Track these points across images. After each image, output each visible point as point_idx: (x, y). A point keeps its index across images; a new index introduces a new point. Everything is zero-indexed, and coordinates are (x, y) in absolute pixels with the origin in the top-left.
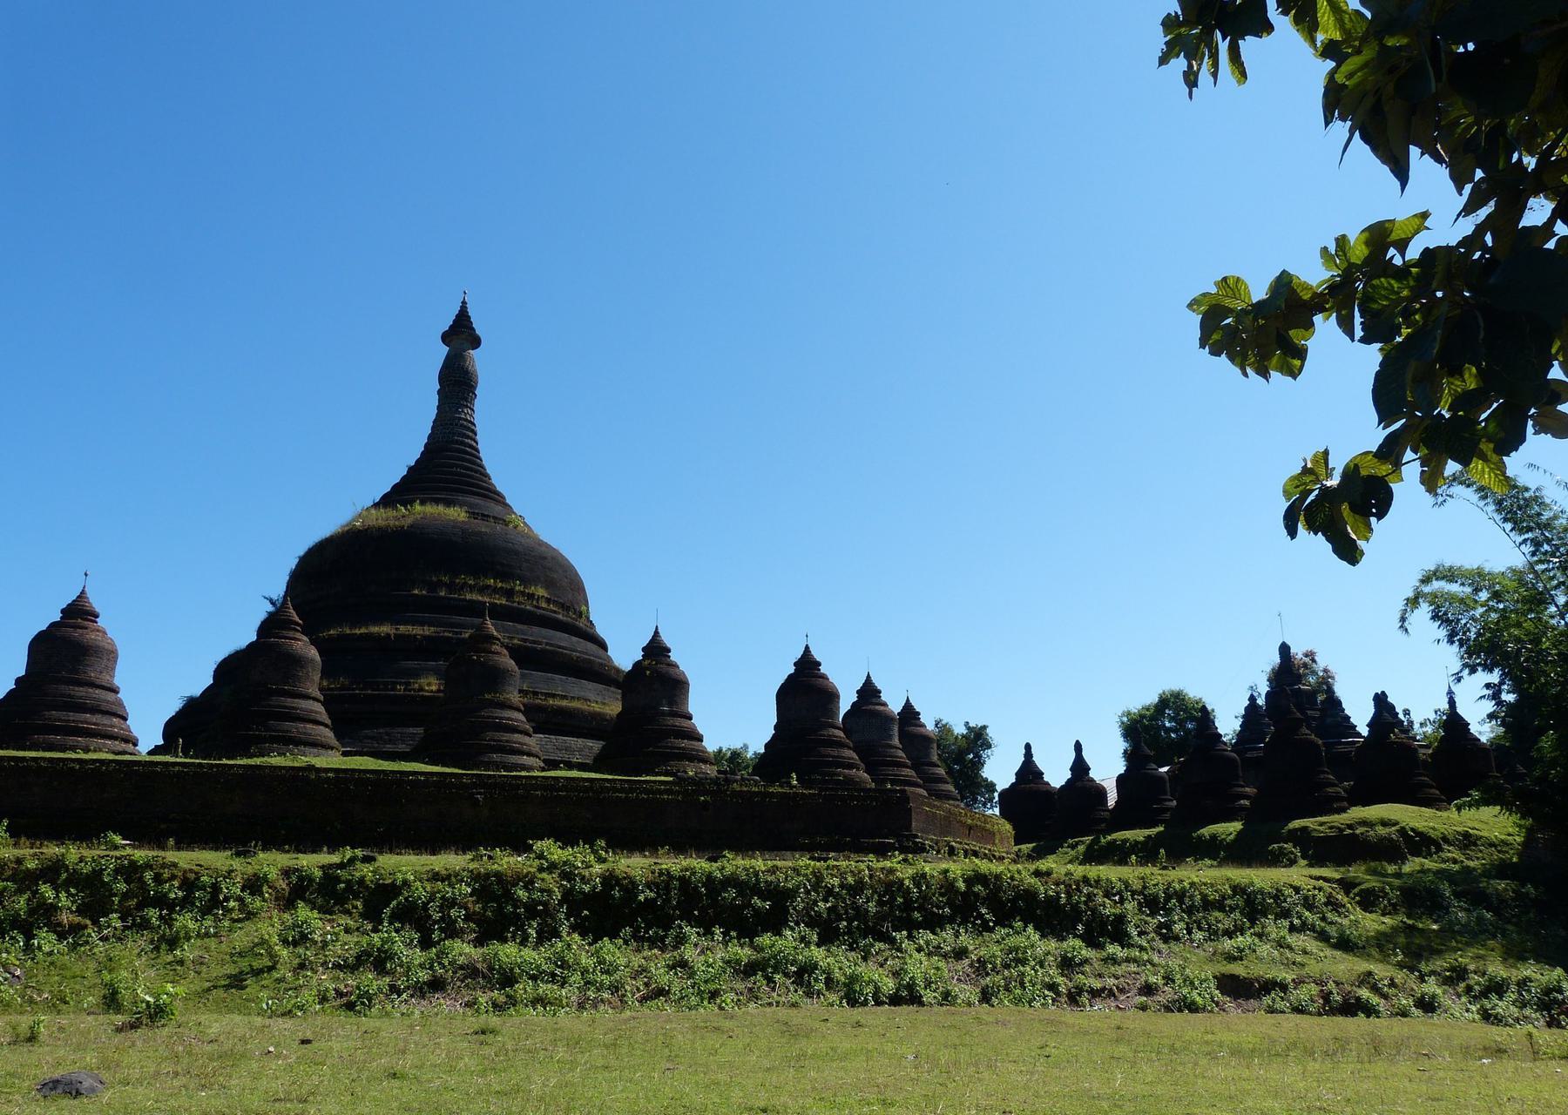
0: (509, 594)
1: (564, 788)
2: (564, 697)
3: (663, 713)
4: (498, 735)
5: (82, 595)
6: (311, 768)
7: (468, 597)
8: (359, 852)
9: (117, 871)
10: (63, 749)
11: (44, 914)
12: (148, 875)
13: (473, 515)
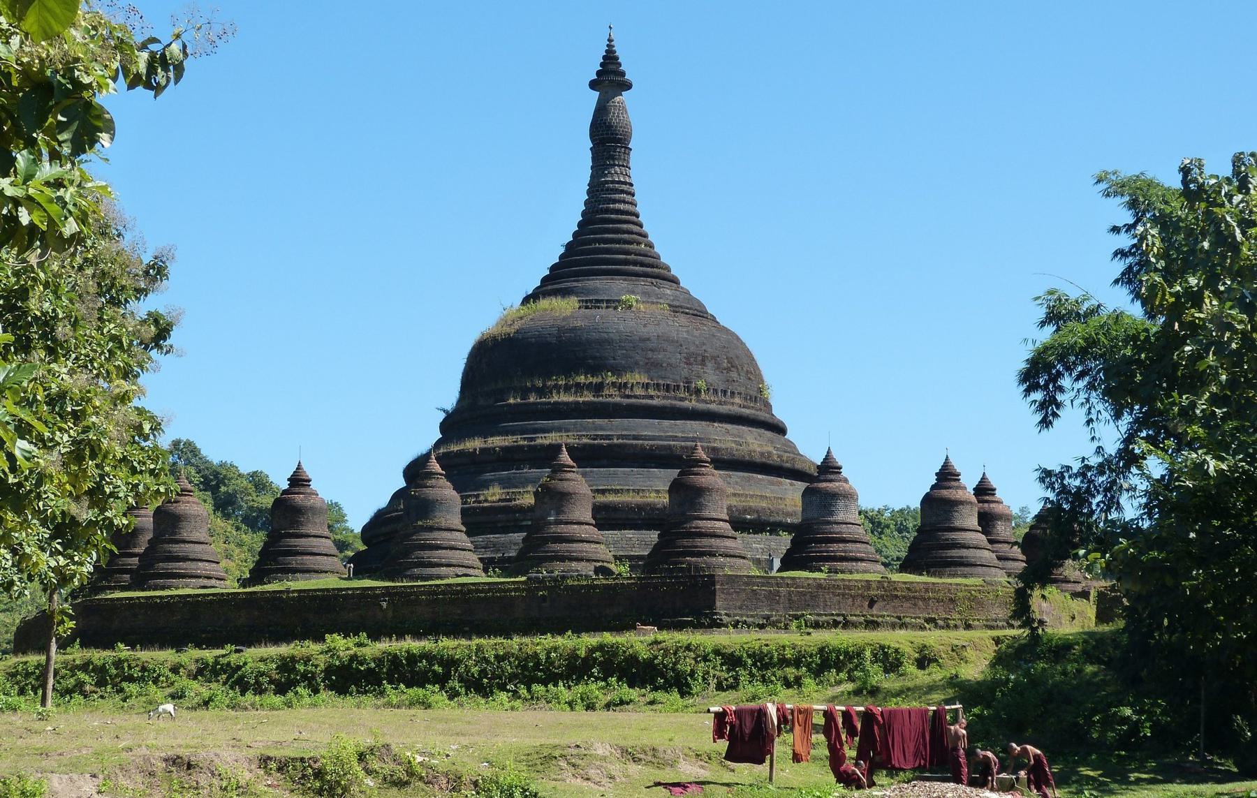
0: (598, 388)
2: (617, 492)
4: (557, 547)
5: (984, 478)
6: (288, 591)
7: (555, 398)
8: (233, 647)
9: (113, 664)
10: (163, 588)
11: (80, 686)
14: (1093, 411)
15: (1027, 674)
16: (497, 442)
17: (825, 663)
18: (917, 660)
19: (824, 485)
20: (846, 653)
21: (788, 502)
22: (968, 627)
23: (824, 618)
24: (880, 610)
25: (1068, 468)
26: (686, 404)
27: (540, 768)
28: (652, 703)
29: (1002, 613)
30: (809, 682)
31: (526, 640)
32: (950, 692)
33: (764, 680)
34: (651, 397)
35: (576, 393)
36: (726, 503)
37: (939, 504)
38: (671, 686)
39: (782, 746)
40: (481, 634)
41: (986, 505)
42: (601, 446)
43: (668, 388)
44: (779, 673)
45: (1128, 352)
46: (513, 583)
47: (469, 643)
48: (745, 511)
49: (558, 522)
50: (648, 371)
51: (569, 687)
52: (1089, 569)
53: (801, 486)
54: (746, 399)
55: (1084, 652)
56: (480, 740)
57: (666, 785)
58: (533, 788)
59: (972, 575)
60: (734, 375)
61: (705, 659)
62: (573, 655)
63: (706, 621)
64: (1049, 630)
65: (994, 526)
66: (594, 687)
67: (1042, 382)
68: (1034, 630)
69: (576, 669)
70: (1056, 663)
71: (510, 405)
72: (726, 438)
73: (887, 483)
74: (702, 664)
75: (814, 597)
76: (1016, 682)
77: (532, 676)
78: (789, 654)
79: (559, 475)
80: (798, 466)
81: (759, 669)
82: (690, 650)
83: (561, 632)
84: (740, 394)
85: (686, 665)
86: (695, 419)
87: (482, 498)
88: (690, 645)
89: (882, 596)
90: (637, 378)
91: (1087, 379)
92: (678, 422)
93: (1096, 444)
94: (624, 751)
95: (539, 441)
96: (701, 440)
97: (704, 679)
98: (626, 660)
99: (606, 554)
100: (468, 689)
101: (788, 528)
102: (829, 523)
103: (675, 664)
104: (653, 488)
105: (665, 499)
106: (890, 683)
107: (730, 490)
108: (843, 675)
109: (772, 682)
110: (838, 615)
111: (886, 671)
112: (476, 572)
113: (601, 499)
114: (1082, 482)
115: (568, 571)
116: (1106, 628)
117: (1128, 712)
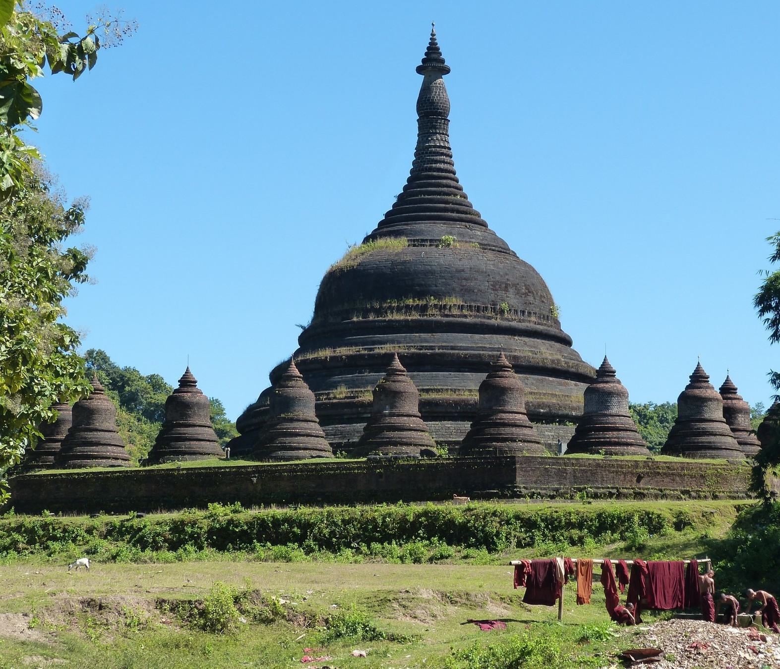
0: (423, 309)
1: (301, 471)
2: (438, 391)
3: (385, 416)
4: (391, 434)
5: (728, 380)
7: (390, 317)
8: (136, 514)
10: (80, 467)
12: (51, 527)
13: (415, 243)
15: (762, 534)
16: (344, 351)
17: (603, 526)
18: (675, 523)
19: (601, 385)
20: (619, 518)
21: (573, 399)
22: (715, 497)
23: (602, 490)
26: (493, 321)
27: (377, 608)
28: (466, 557)
29: (742, 486)
30: (589, 541)
31: (367, 508)
32: (701, 549)
34: (465, 316)
35: (406, 313)
36: (524, 399)
37: (692, 401)
39: (568, 592)
40: (330, 503)
41: (729, 401)
42: (425, 355)
43: (478, 309)
44: (566, 534)
46: (356, 462)
47: (321, 510)
48: (540, 406)
49: (392, 415)
50: (462, 296)
51: (401, 545)
53: (584, 386)
54: (540, 317)
56: (330, 586)
58: (372, 624)
60: (531, 299)
61: (508, 522)
62: (404, 520)
63: (509, 493)
65: (736, 418)
66: (420, 544)
69: (406, 531)
71: (354, 321)
72: (524, 348)
73: (650, 385)
74: (506, 527)
75: (594, 474)
77: (372, 535)
78: (574, 518)
80: (581, 370)
81: (551, 531)
82: (496, 516)
83: (394, 501)
84: (535, 313)
85: (493, 527)
87: (332, 396)
88: (495, 511)
89: (647, 473)
90: (453, 301)
92: (486, 336)
94: (444, 595)
95: (377, 351)
96: (504, 350)
97: (507, 538)
98: (445, 523)
100: (320, 546)
101: (573, 419)
103: (484, 527)
104: (467, 388)
105: (476, 397)
106: (654, 541)
107: (528, 390)
109: (560, 541)
110: (612, 488)
115: (400, 453)
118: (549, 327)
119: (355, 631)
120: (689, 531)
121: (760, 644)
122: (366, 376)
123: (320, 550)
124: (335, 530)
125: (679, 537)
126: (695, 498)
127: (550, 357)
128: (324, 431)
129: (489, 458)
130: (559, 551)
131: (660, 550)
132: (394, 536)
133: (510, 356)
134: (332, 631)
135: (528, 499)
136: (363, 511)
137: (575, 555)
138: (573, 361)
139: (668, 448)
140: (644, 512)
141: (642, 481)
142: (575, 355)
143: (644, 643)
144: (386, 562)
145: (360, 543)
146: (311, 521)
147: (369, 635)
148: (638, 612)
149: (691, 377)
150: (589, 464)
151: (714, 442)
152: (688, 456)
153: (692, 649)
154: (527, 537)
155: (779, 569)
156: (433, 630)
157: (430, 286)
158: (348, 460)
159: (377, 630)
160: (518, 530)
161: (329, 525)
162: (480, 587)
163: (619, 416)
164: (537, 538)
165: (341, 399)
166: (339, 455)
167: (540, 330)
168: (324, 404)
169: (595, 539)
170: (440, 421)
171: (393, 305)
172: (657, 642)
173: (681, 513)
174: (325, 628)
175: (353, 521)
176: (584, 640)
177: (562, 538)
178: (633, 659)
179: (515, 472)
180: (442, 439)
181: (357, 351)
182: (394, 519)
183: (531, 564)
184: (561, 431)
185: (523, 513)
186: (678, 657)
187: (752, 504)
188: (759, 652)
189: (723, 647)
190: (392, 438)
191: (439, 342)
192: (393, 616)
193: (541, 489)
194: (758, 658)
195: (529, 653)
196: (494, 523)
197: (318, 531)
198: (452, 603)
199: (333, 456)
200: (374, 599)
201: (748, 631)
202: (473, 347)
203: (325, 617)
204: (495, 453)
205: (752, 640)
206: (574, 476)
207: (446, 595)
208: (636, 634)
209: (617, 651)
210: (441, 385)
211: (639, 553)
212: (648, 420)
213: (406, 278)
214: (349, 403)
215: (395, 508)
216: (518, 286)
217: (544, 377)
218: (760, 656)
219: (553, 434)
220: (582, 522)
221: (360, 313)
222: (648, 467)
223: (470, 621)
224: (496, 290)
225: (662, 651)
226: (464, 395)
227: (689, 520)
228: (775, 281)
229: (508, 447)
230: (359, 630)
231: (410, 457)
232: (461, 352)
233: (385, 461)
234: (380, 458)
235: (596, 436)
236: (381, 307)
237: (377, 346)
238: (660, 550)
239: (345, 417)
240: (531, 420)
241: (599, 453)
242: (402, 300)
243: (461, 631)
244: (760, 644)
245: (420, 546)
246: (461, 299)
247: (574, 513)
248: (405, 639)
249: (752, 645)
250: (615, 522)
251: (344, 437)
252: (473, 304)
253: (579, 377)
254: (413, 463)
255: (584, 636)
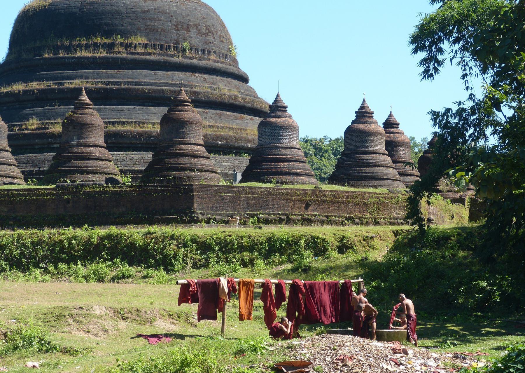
0: (110, 47)
2: (123, 123)
3: (73, 146)
4: (79, 163)
5: (390, 116)
7: (79, 54)
14: (467, 68)
15: (413, 257)
16: (35, 85)
17: (272, 249)
18: (338, 247)
19: (274, 119)
20: (287, 242)
21: (249, 132)
22: (377, 223)
23: (273, 216)
24: (313, 211)
25: (449, 110)
26: (175, 59)
27: (53, 323)
28: (145, 277)
29: (401, 213)
30: (260, 263)
31: (55, 231)
32: (361, 271)
33: (227, 261)
34: (149, 54)
35: (94, 50)
36: (203, 132)
37: (357, 134)
38: (159, 265)
39: (231, 308)
40: (20, 227)
41: (392, 135)
42: (112, 90)
43: (161, 47)
44: (238, 256)
45: (491, 23)
46: (46, 189)
47: (12, 233)
48: (217, 138)
49: (79, 145)
50: (147, 35)
51: (85, 266)
52: (457, 184)
53: (258, 120)
54: (219, 56)
55: (458, 241)
56: (10, 303)
57: (146, 337)
58: (47, 338)
59: (380, 186)
60: (210, 38)
61: (185, 245)
62: (88, 242)
63: (186, 218)
64: (433, 226)
65: (397, 151)
66: (103, 265)
67: (427, 44)
68: (422, 226)
69: (91, 252)
70: (438, 249)
71: (45, 58)
72: (203, 84)
73: (318, 119)
74: (183, 249)
75: (265, 201)
76: (406, 264)
77: (58, 257)
78: (245, 242)
79: (80, 111)
80: (257, 106)
81: (224, 253)
82: (174, 239)
83: (80, 225)
84: (215, 52)
85: (171, 249)
86: (181, 71)
87: (24, 127)
88: (174, 235)
89: (315, 201)
90: (140, 40)
91: (461, 43)
92: (169, 73)
93: (469, 92)
94: (116, 312)
95: (66, 86)
96: (185, 86)
97: (184, 260)
98: (127, 246)
99: (113, 168)
100: (11, 266)
101: (248, 151)
102: (277, 147)
103: (162, 249)
104: (149, 121)
105: (158, 129)
106: (318, 263)
107: (206, 123)
108: (284, 258)
109: (233, 262)
110: (283, 214)
111: (316, 255)
112: (19, 181)
113: (111, 128)
114: (460, 120)
115: (86, 181)
116: (474, 225)
117: (484, 284)
118: (227, 65)
119: (31, 344)
120: (350, 254)
121: (402, 357)
122: (57, 109)
123: (10, 270)
124: (24, 252)
125: (341, 260)
126: (358, 224)
127: (228, 93)
128: (16, 159)
129: (169, 186)
130: (232, 272)
131: (323, 271)
132: (79, 258)
133: (190, 91)
134: (10, 344)
135: (204, 224)
136: (51, 234)
137: (242, 275)
138: (248, 97)
139: (333, 179)
140: (310, 237)
141: (310, 208)
142: (251, 92)
143: (295, 356)
144: (71, 281)
145: (48, 264)
146: (3, 243)
147: (44, 349)
148: (296, 327)
149: (356, 112)
150: (262, 192)
151: (376, 173)
152: (353, 186)
153: (340, 362)
154: (203, 259)
155: (428, 289)
156: (103, 344)
157: (117, 25)
158: (38, 187)
159: (51, 343)
160: (194, 252)
161: (19, 246)
162: (151, 304)
163: (290, 148)
164: (211, 260)
165: (33, 130)
166: (30, 182)
167: (219, 68)
168: (17, 134)
169: (264, 261)
170: (125, 151)
171: (82, 43)
172: (307, 355)
173: (344, 237)
174: (4, 341)
175: (42, 243)
176: (240, 353)
177: (234, 260)
178: (285, 370)
179: (193, 199)
180: (126, 168)
181: (48, 86)
182: (79, 242)
183: (196, 284)
184: (237, 162)
185: (199, 237)
186: (326, 368)
187: (409, 230)
188: (401, 364)
189: (367, 359)
190: (79, 166)
191: (124, 78)
192: (67, 330)
193: (217, 215)
194: (399, 369)
195: (188, 365)
196: (172, 246)
197: (9, 252)
198: (123, 319)
199: (24, 183)
200: (51, 315)
201: (392, 345)
202: (157, 83)
203: (4, 331)
204: (175, 182)
205: (395, 353)
206: (247, 203)
207: (118, 311)
208: (289, 347)
209: (270, 363)
210: (126, 118)
211: (304, 274)
212: (323, 153)
213: (94, 18)
214: (40, 134)
215: (80, 231)
216: (199, 27)
217: (221, 112)
218: (402, 367)
219: (229, 164)
220: (253, 246)
221: (51, 50)
222: (316, 195)
223: (140, 336)
224: (179, 30)
225: (311, 363)
226: (148, 127)
227: (351, 244)
228: (430, 22)
229: (187, 176)
230: (35, 343)
231: (96, 184)
232: (145, 87)
233: (72, 188)
234: (68, 185)
235: (268, 167)
236: (71, 44)
237: (66, 81)
238: (323, 271)
239: (36, 147)
240: (210, 152)
241: (271, 182)
242: (90, 38)
243: (130, 344)
244: (402, 357)
245: (103, 266)
246: (146, 38)
247: (246, 237)
248: (77, 351)
249: (395, 357)
250: (283, 245)
251: (36, 166)
252: (156, 43)
253: (254, 112)
254: (98, 190)
255: (240, 350)
